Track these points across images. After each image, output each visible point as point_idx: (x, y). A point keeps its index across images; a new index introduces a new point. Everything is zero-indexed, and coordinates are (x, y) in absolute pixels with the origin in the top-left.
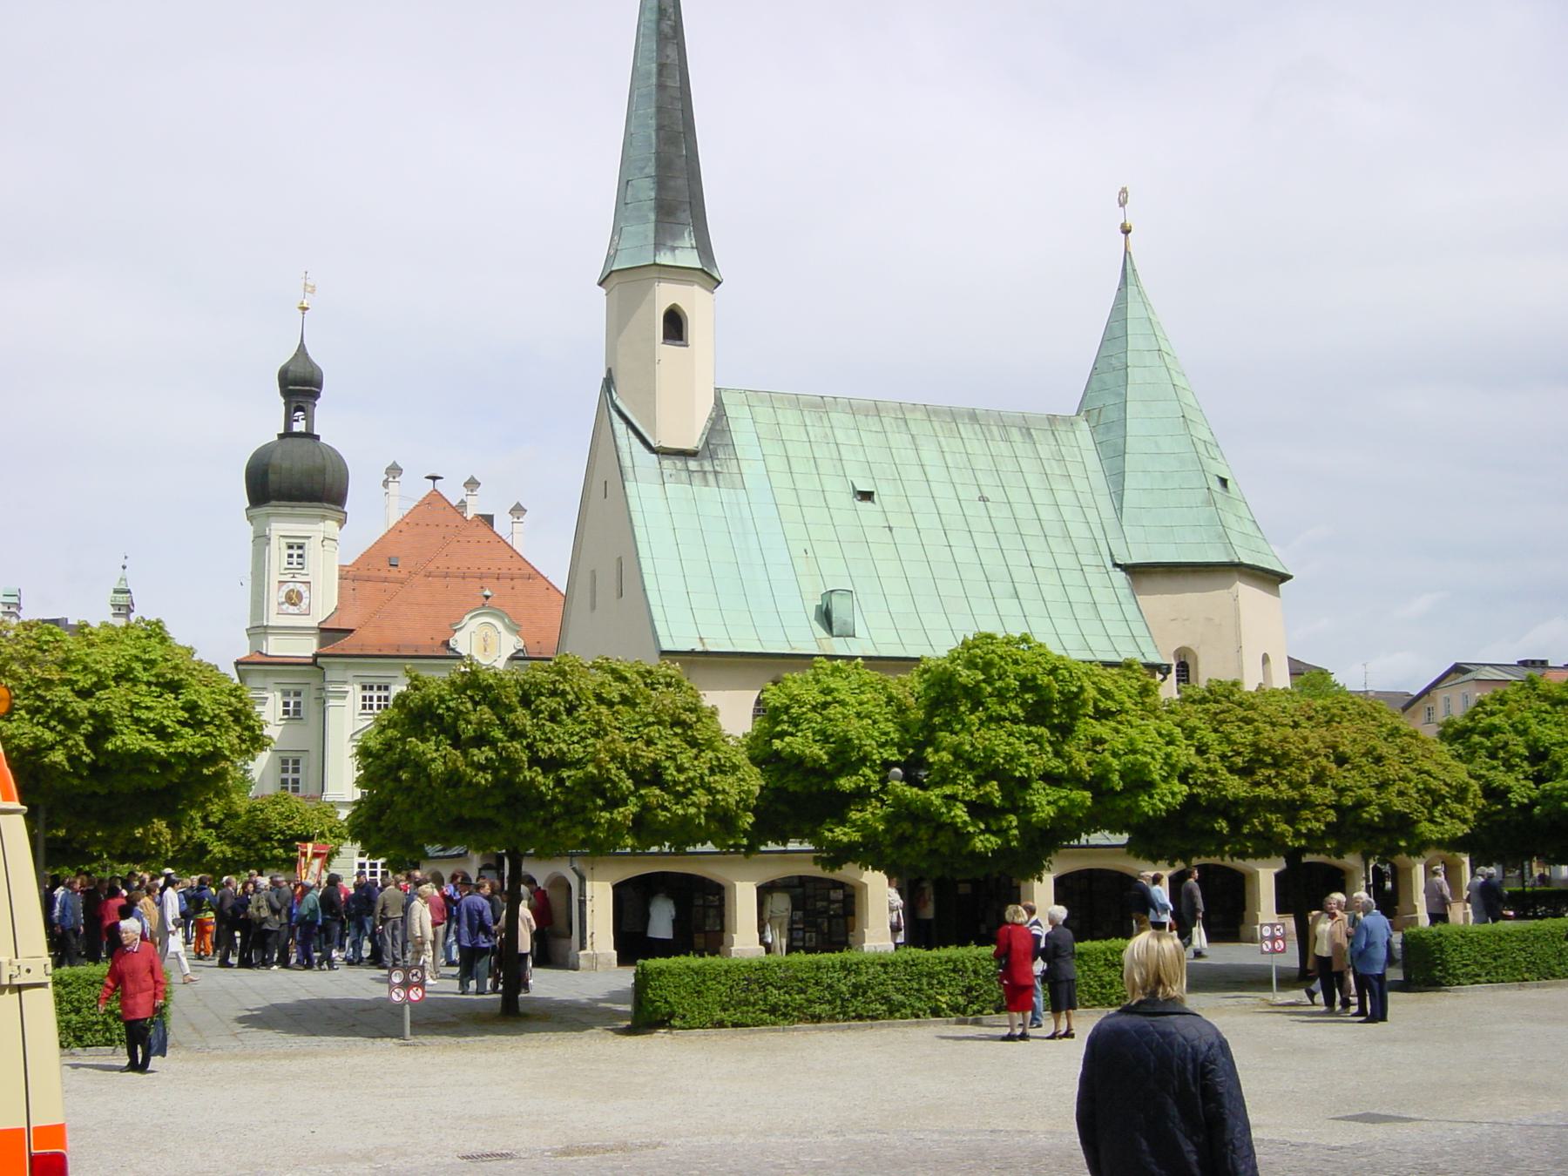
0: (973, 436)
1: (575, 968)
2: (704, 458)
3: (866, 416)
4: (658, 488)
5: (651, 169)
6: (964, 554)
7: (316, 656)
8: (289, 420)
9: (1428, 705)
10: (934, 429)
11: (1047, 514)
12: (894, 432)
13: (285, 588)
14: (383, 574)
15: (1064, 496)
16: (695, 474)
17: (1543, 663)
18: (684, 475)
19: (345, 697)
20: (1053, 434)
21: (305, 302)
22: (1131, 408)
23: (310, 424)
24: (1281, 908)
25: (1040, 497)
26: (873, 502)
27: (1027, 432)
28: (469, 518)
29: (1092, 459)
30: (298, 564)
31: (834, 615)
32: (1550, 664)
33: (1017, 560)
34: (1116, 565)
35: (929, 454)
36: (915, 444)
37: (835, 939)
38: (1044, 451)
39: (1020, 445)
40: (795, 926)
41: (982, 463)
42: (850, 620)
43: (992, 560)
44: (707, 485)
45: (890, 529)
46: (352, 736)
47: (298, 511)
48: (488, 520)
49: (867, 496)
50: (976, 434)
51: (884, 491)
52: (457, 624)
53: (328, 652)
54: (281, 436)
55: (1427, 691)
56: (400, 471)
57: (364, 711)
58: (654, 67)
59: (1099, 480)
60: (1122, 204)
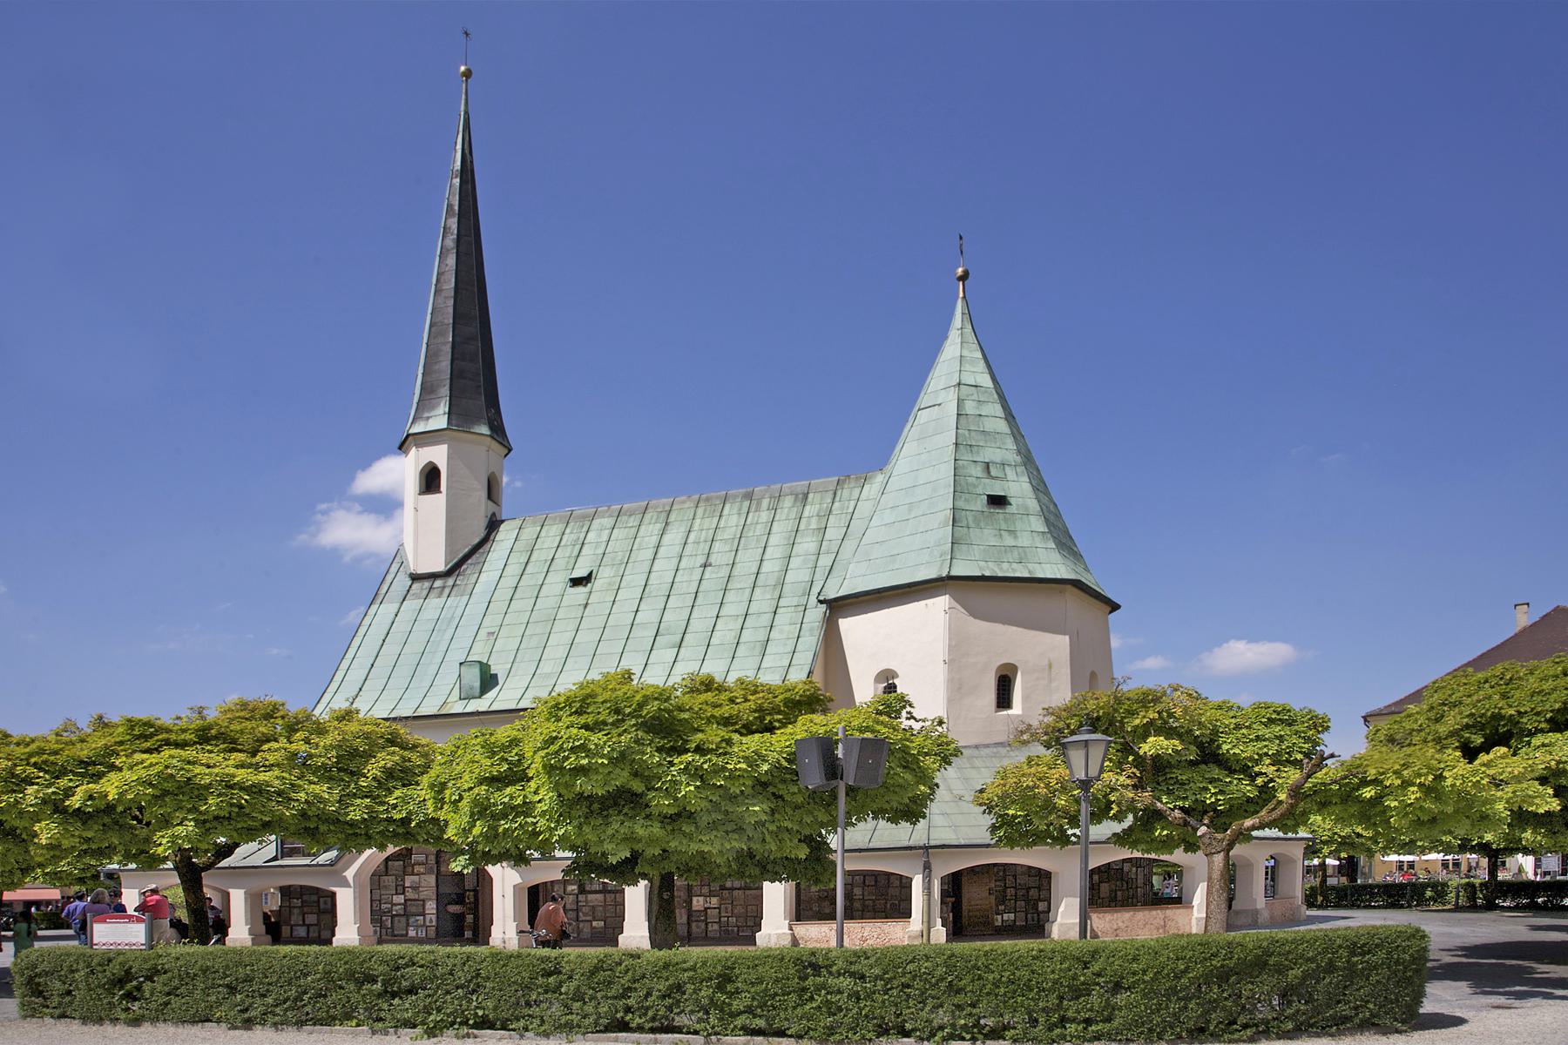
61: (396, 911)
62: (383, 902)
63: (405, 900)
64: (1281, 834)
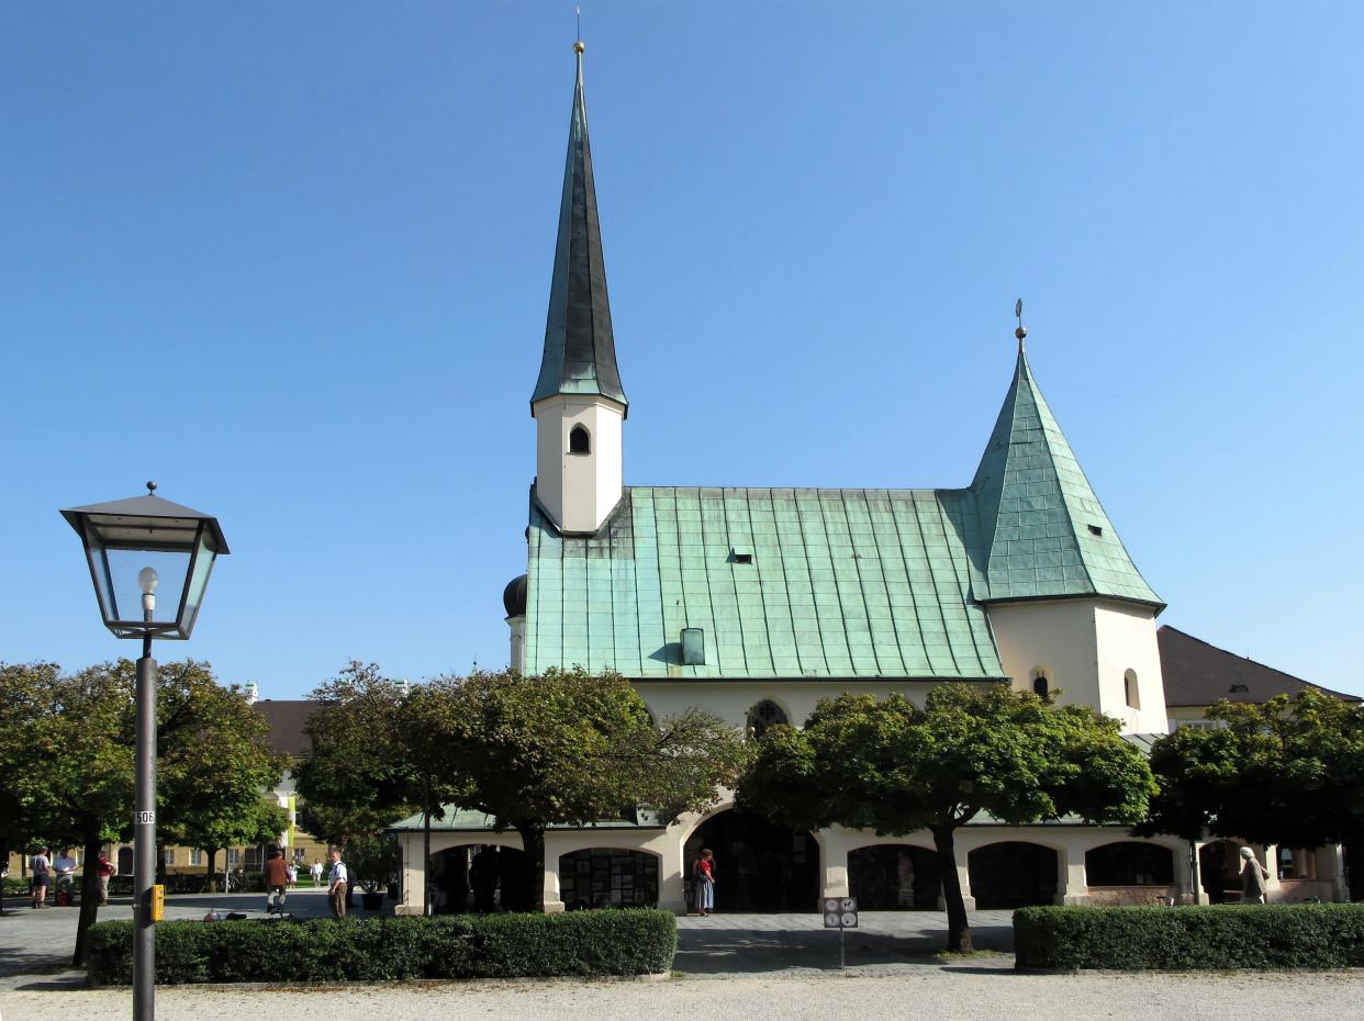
6: (825, 597)
27: (913, 503)
39: (903, 515)
40: (626, 887)
42: (700, 651)
51: (765, 557)
56: (219, 546)
60: (1018, 314)
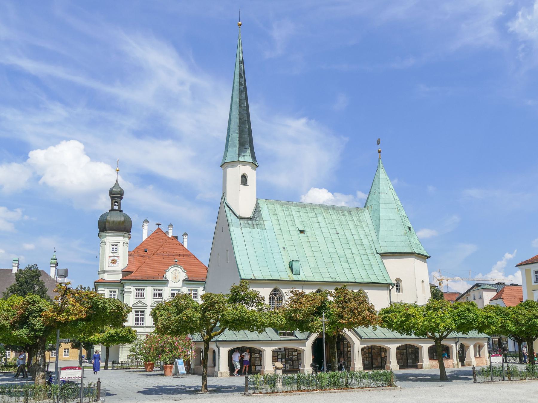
0: (333, 214)
1: (217, 376)
2: (253, 220)
3: (302, 207)
4: (240, 229)
5: (237, 131)
6: (331, 250)
7: (121, 280)
8: (112, 206)
9: (467, 296)
10: (322, 211)
11: (356, 237)
12: (310, 212)
13: (111, 259)
14: (142, 254)
15: (361, 232)
16: (251, 225)
17: (504, 283)
18: (247, 225)
19: (131, 293)
20: (358, 213)
21: (118, 168)
22: (382, 205)
23: (119, 207)
24: (431, 358)
25: (354, 232)
26: (304, 234)
27: (350, 213)
28: (170, 237)
29: (369, 221)
30: (115, 251)
31: (293, 268)
32: (518, 285)
33: (348, 251)
34: (377, 253)
35: (321, 219)
36: (317, 216)
37: (294, 367)
38: (355, 218)
39: (348, 217)
41: (336, 222)
42: (298, 269)
43: (340, 251)
44: (254, 228)
45: (309, 242)
46: (132, 305)
47: (115, 234)
48: (176, 237)
49: (302, 232)
50: (334, 213)
51: (307, 230)
52: (166, 270)
53: (125, 279)
54: (110, 211)
55: (467, 292)
57: (136, 298)
58: (238, 100)
59: (371, 227)
60: (378, 143)
61: (294, 358)
62: (289, 354)
63: (297, 354)
64: (417, 337)
